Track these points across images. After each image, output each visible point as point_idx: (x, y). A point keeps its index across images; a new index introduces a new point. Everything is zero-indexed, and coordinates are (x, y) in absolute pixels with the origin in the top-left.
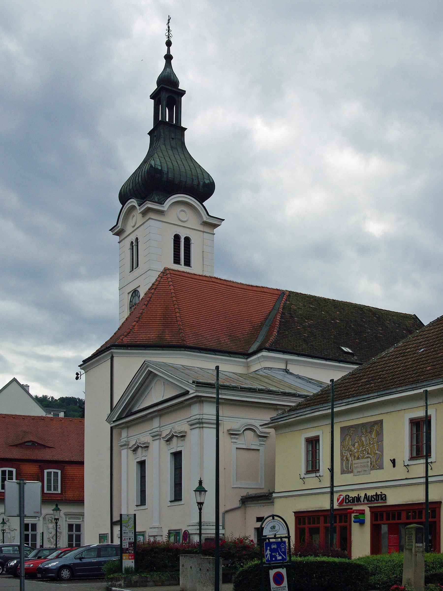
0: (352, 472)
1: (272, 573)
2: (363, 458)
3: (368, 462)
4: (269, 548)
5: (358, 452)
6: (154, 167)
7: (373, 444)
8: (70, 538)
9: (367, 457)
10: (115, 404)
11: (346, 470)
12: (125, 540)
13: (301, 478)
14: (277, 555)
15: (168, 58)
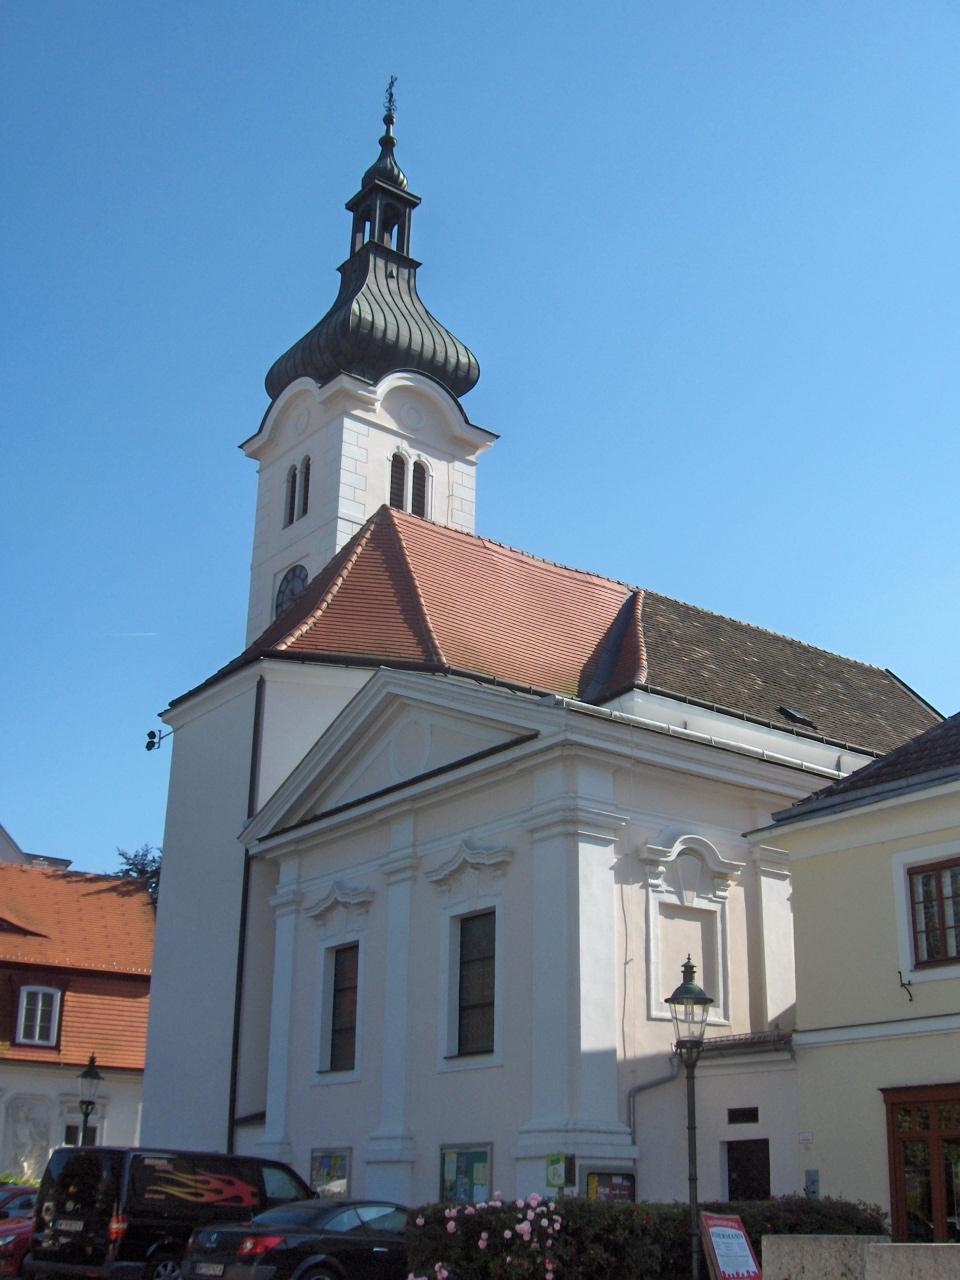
10: (265, 793)
13: (903, 985)
15: (387, 143)
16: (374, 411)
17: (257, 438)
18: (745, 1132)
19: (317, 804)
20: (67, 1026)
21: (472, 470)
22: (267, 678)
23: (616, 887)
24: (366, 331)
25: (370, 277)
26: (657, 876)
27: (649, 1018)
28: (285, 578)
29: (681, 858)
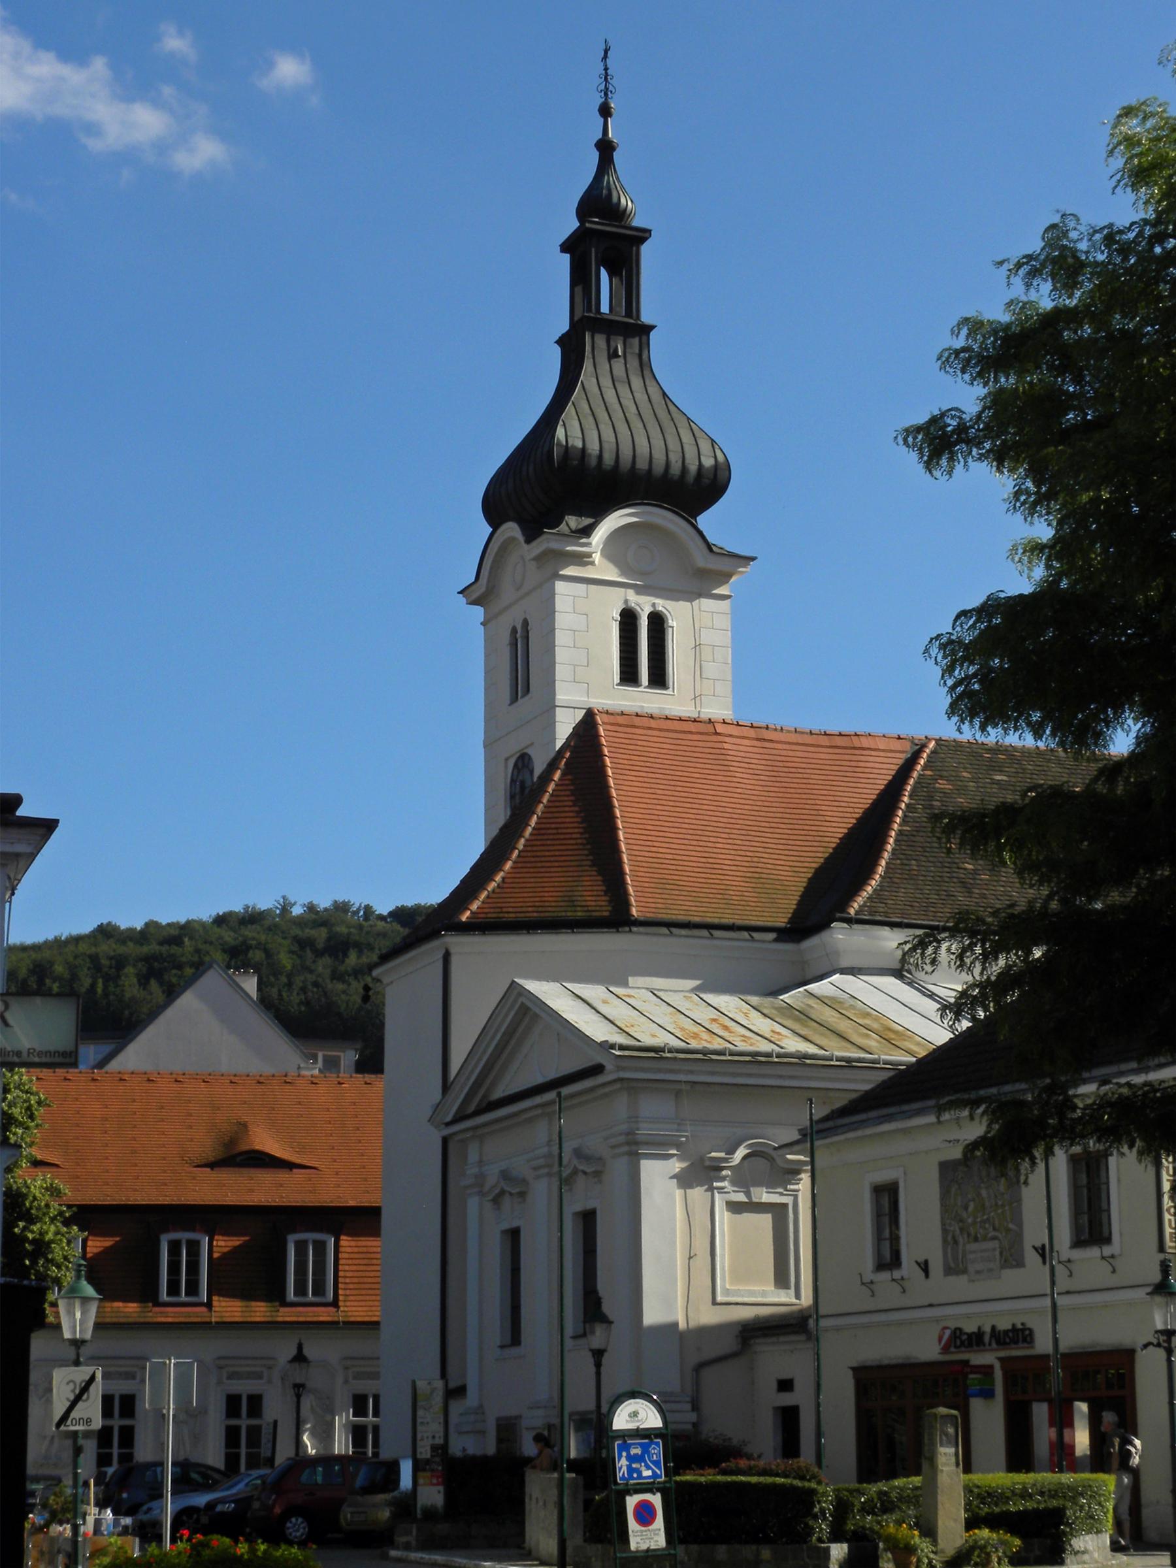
0: (964, 1271)
1: (632, 1502)
2: (985, 1239)
3: (994, 1249)
4: (624, 1454)
5: (974, 1223)
6: (564, 443)
7: (1003, 1206)
8: (232, 1436)
9: (994, 1238)
11: (952, 1265)
12: (422, 1439)
13: (863, 1284)
14: (643, 1468)
15: (606, 148)
16: (592, 563)
17: (474, 587)
18: (787, 1399)
19: (494, 1084)
20: (345, 1277)
21: (725, 605)
22: (452, 951)
23: (678, 1193)
24: (576, 462)
25: (588, 365)
26: (723, 1179)
27: (714, 1303)
28: (516, 765)
29: (746, 1162)
